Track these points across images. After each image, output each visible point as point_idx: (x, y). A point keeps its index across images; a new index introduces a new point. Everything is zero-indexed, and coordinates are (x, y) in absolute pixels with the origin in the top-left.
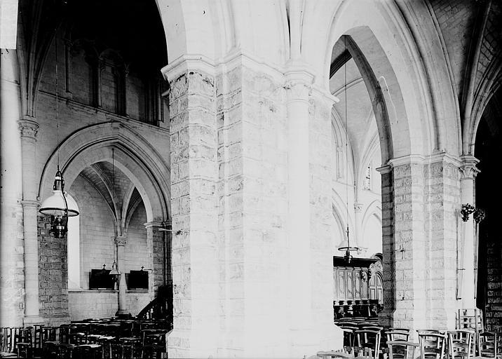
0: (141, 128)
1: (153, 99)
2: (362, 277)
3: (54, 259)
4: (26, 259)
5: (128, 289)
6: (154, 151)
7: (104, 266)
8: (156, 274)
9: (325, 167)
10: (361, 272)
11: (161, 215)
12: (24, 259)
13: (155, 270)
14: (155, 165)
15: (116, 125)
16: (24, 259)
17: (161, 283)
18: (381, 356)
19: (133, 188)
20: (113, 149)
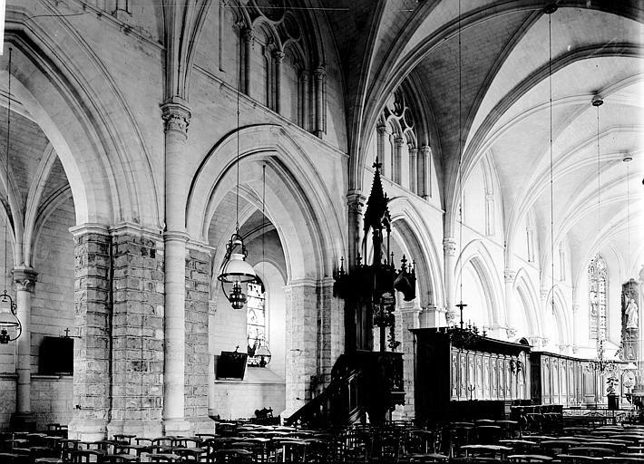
0: (303, 139)
1: (310, 100)
2: (512, 369)
3: (201, 328)
4: (169, 326)
5: (217, 379)
6: (58, 70)
7: (67, 331)
8: (306, 357)
9: (100, 15)
10: (511, 362)
11: (315, 270)
12: (165, 325)
13: (307, 350)
14: (315, 195)
15: (276, 129)
16: (165, 325)
17: (314, 373)
18: (643, 444)
19: (52, 160)
20: (264, 167)
